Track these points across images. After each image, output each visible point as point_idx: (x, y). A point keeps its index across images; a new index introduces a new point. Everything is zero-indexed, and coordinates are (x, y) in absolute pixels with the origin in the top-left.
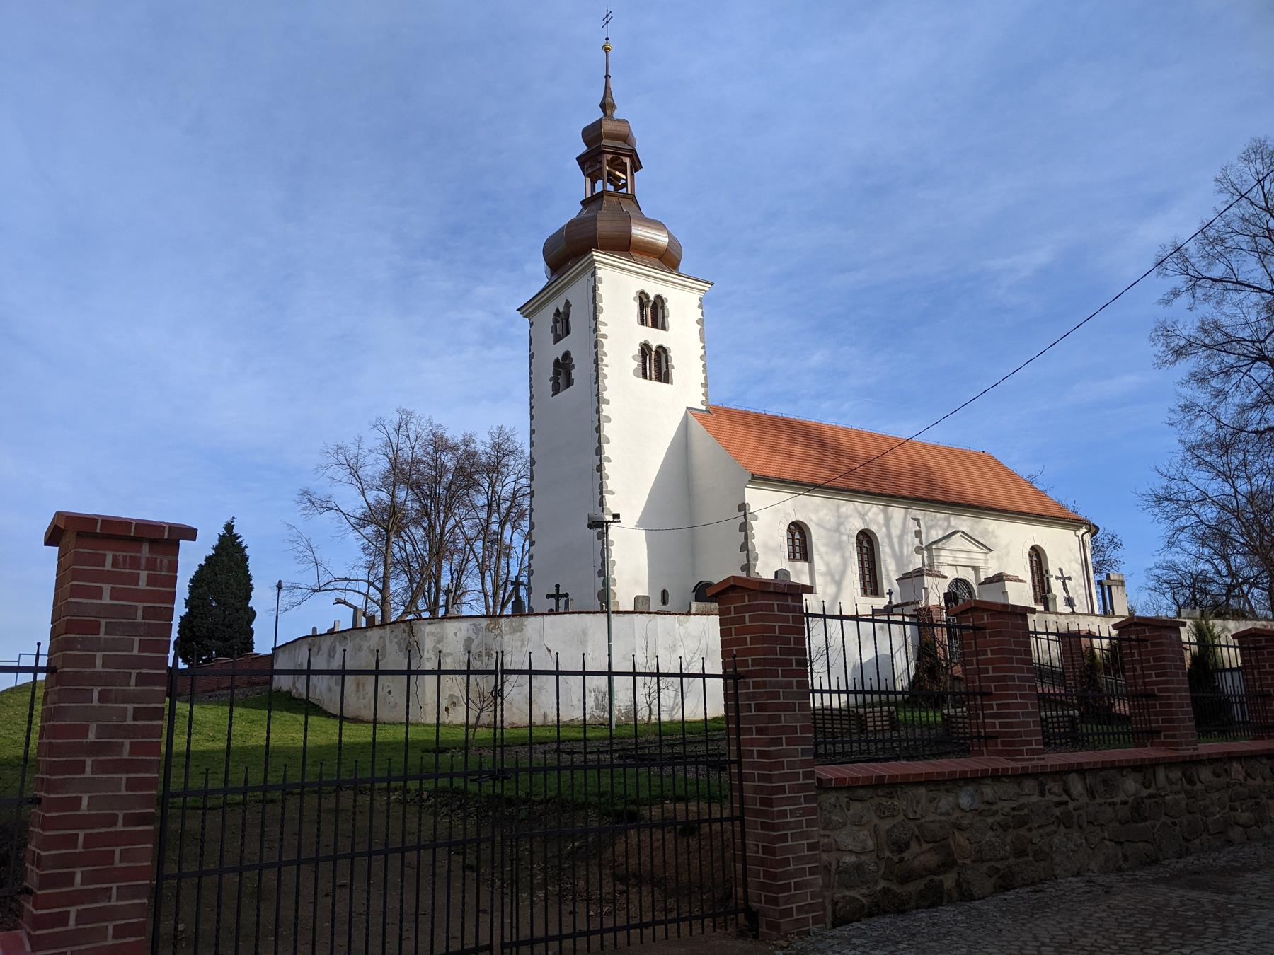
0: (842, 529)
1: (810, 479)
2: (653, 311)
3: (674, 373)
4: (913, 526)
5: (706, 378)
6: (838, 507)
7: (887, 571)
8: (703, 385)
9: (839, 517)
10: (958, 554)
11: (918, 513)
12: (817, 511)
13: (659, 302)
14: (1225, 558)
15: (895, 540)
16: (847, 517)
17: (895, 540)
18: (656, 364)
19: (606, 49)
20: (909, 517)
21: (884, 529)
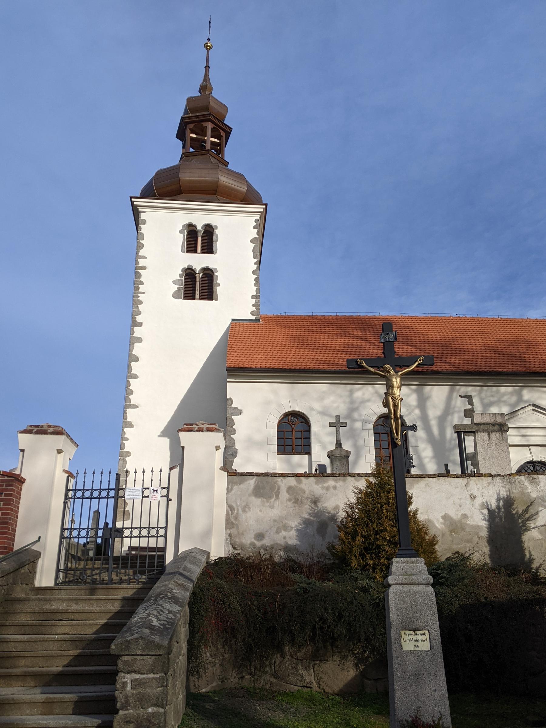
0: (356, 415)
1: (311, 365)
2: (201, 240)
3: (219, 290)
4: (460, 404)
5: (257, 290)
6: (351, 392)
7: (419, 457)
8: (253, 297)
9: (352, 402)
10: (529, 432)
11: (470, 390)
12: (321, 399)
13: (209, 231)
14: (350, 719)
15: (434, 423)
16: (363, 402)
17: (434, 423)
18: (199, 286)
19: (208, 48)
20: (455, 394)
21: (417, 412)
